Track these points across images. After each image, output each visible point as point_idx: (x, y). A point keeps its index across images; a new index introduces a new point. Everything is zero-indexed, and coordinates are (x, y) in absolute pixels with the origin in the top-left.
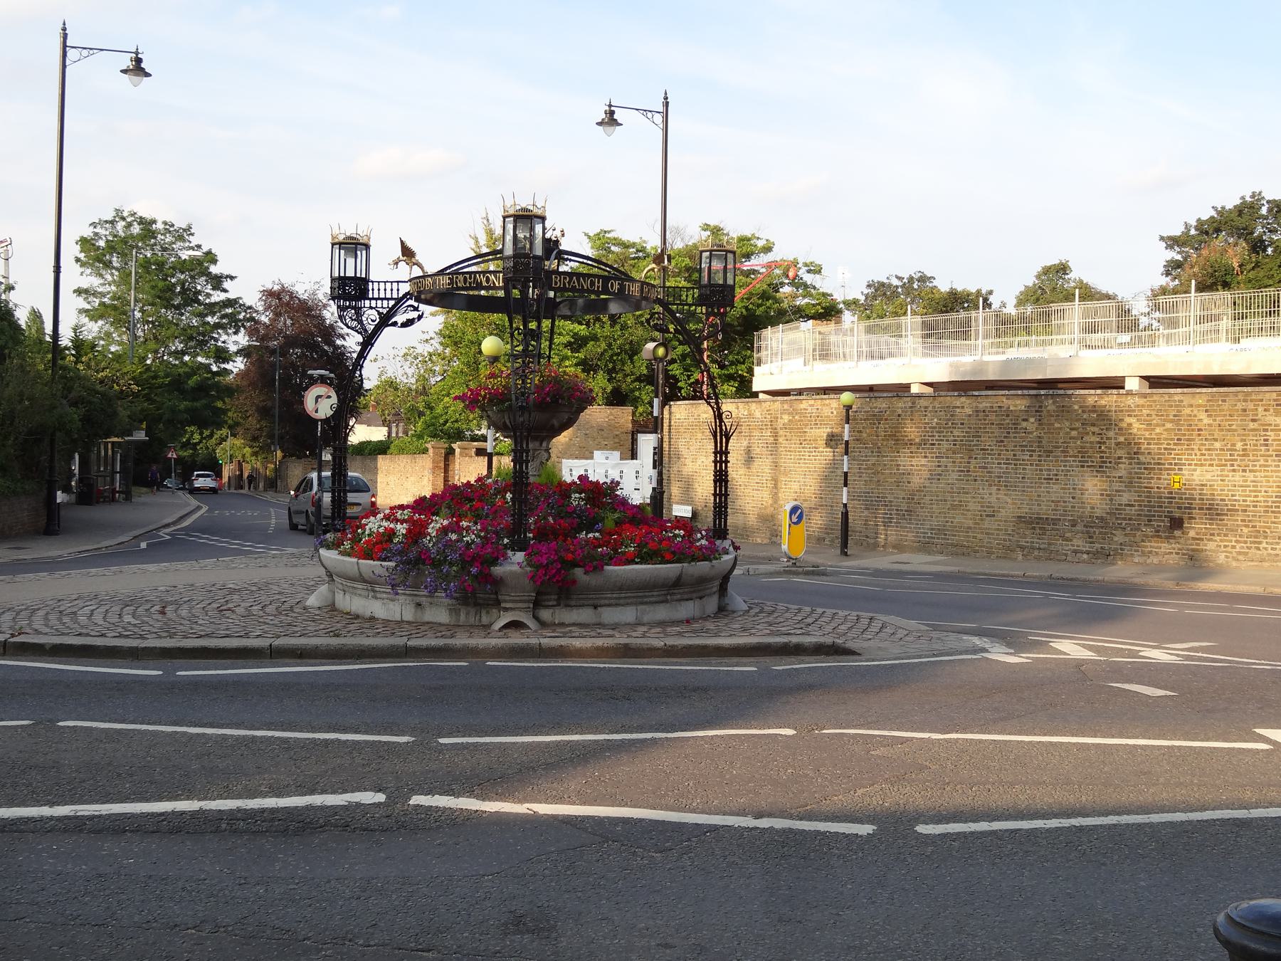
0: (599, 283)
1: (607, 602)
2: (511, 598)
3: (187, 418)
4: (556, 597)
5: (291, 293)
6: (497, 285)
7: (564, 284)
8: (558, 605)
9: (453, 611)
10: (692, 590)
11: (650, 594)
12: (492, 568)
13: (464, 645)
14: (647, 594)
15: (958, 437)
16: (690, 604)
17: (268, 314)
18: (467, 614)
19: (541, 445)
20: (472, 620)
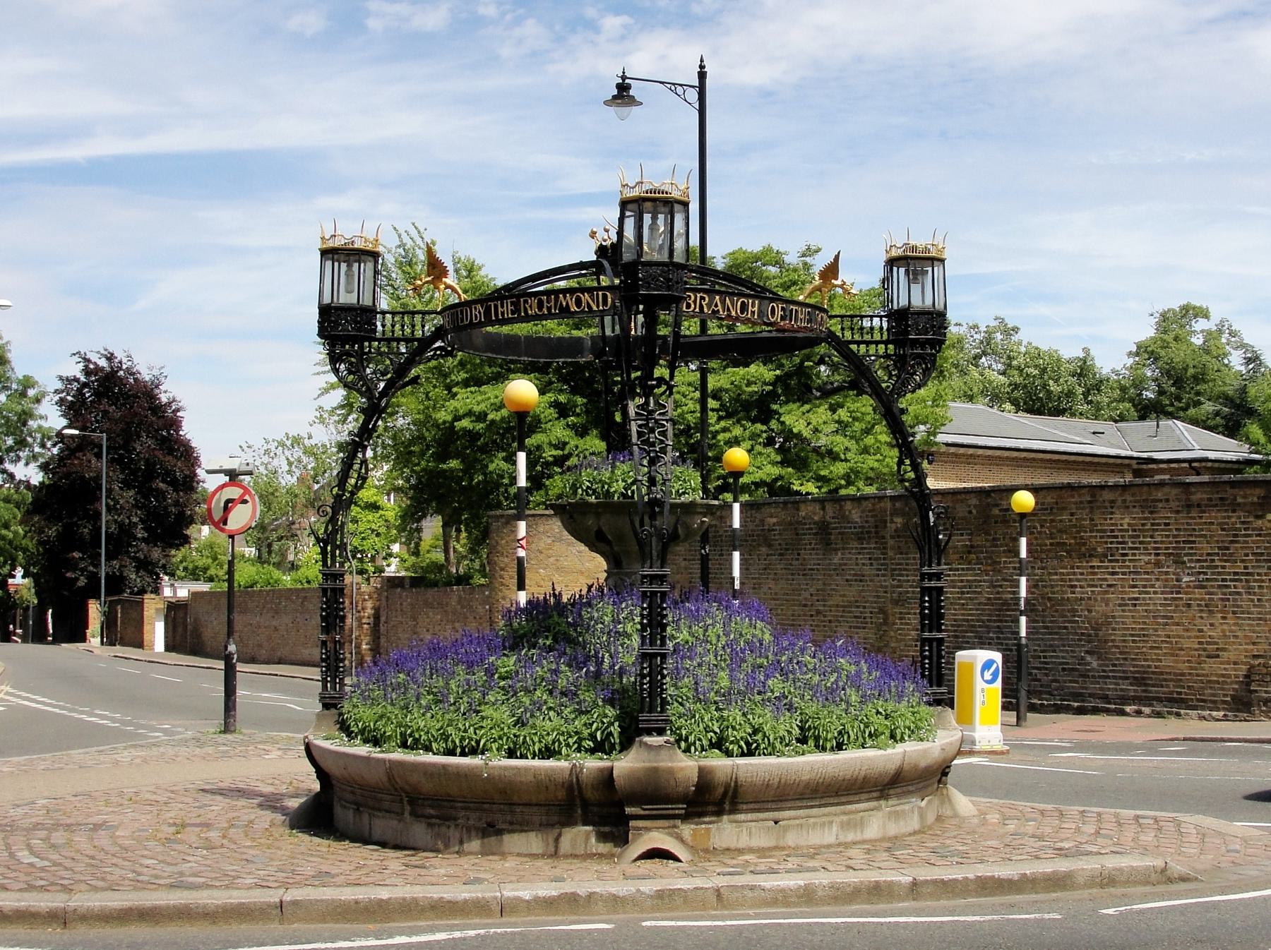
0: (753, 306)
6: (595, 308)
15: (1162, 542)
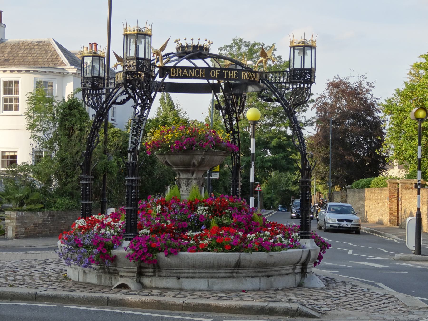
1: (186, 275)
2: (124, 270)
3: (270, 165)
4: (152, 270)
5: (345, 84)
7: (179, 74)
8: (154, 275)
9: (99, 277)
10: (256, 270)
11: (218, 271)
12: (112, 250)
13: (67, 295)
14: (215, 271)
16: (257, 280)
17: (331, 97)
18: (105, 279)
19: (192, 175)
20: (108, 283)
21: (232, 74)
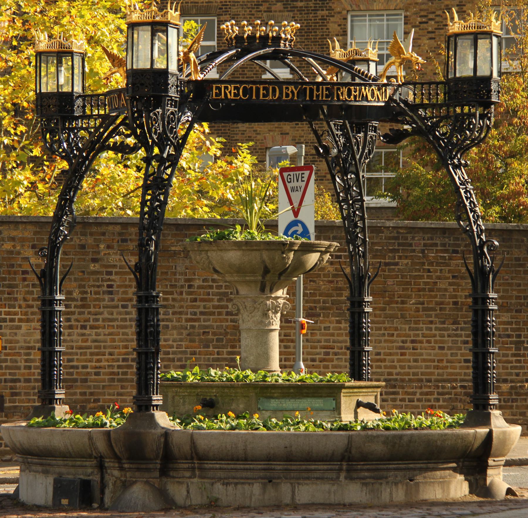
21: (320, 92)
